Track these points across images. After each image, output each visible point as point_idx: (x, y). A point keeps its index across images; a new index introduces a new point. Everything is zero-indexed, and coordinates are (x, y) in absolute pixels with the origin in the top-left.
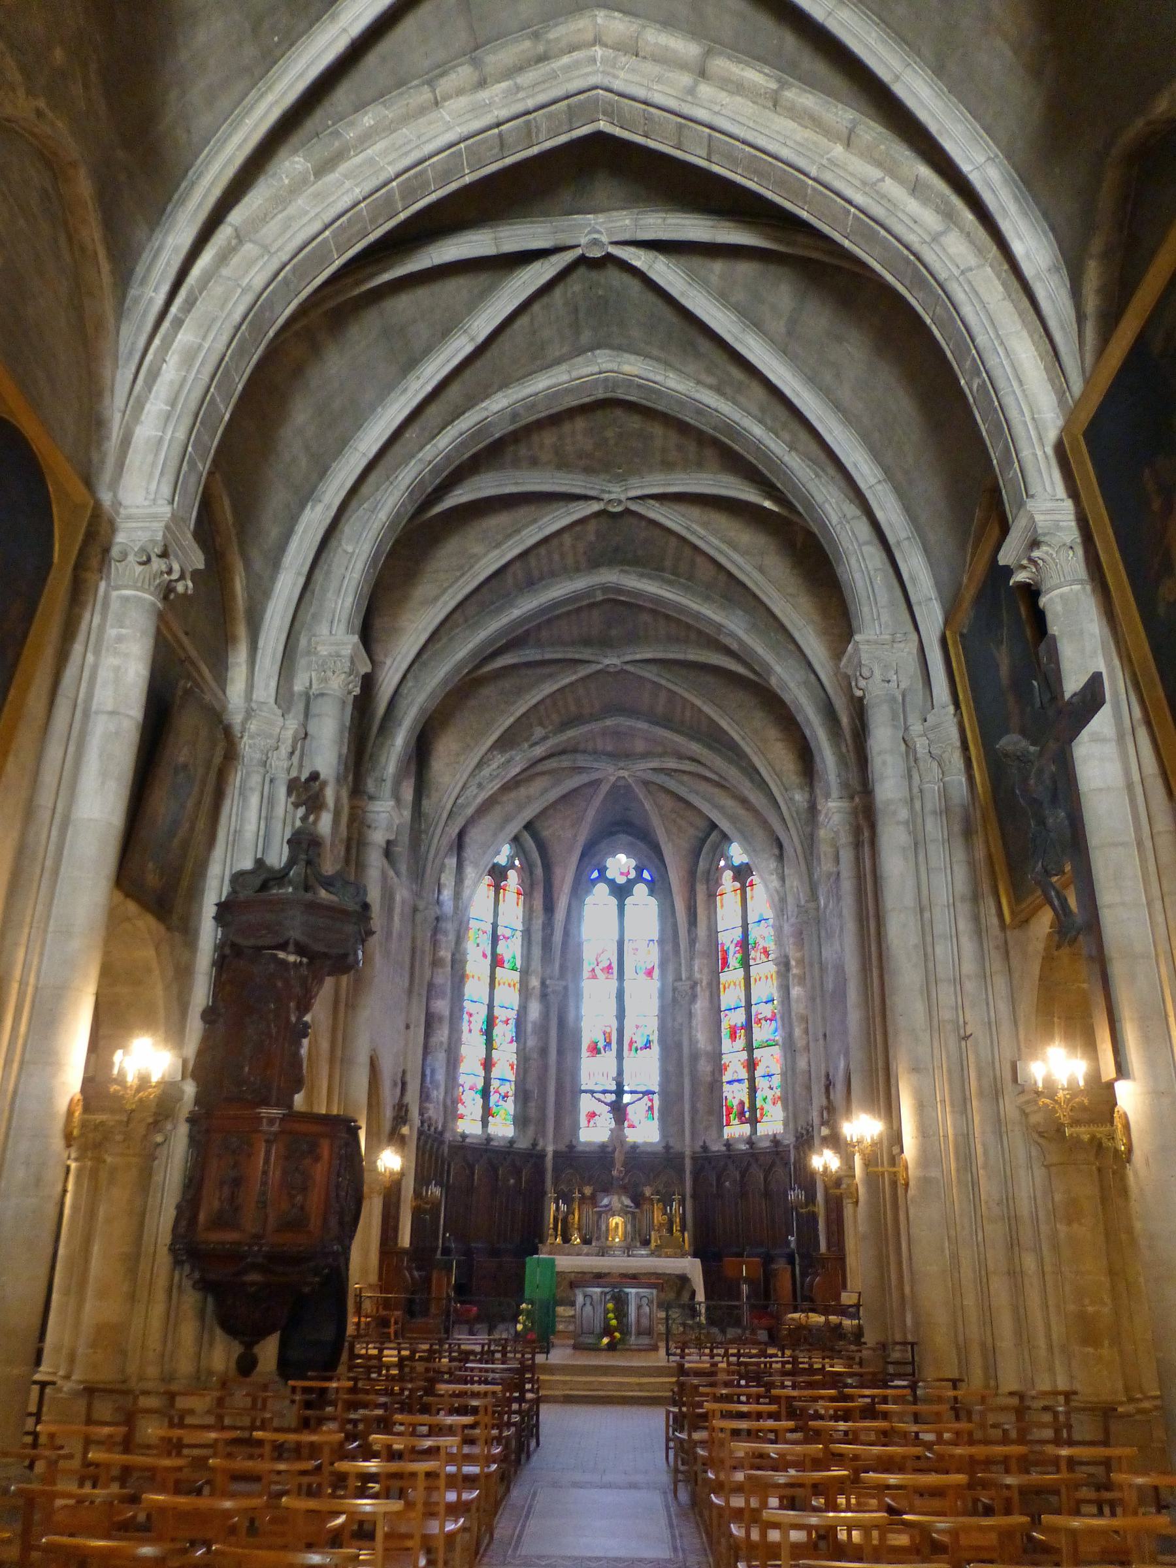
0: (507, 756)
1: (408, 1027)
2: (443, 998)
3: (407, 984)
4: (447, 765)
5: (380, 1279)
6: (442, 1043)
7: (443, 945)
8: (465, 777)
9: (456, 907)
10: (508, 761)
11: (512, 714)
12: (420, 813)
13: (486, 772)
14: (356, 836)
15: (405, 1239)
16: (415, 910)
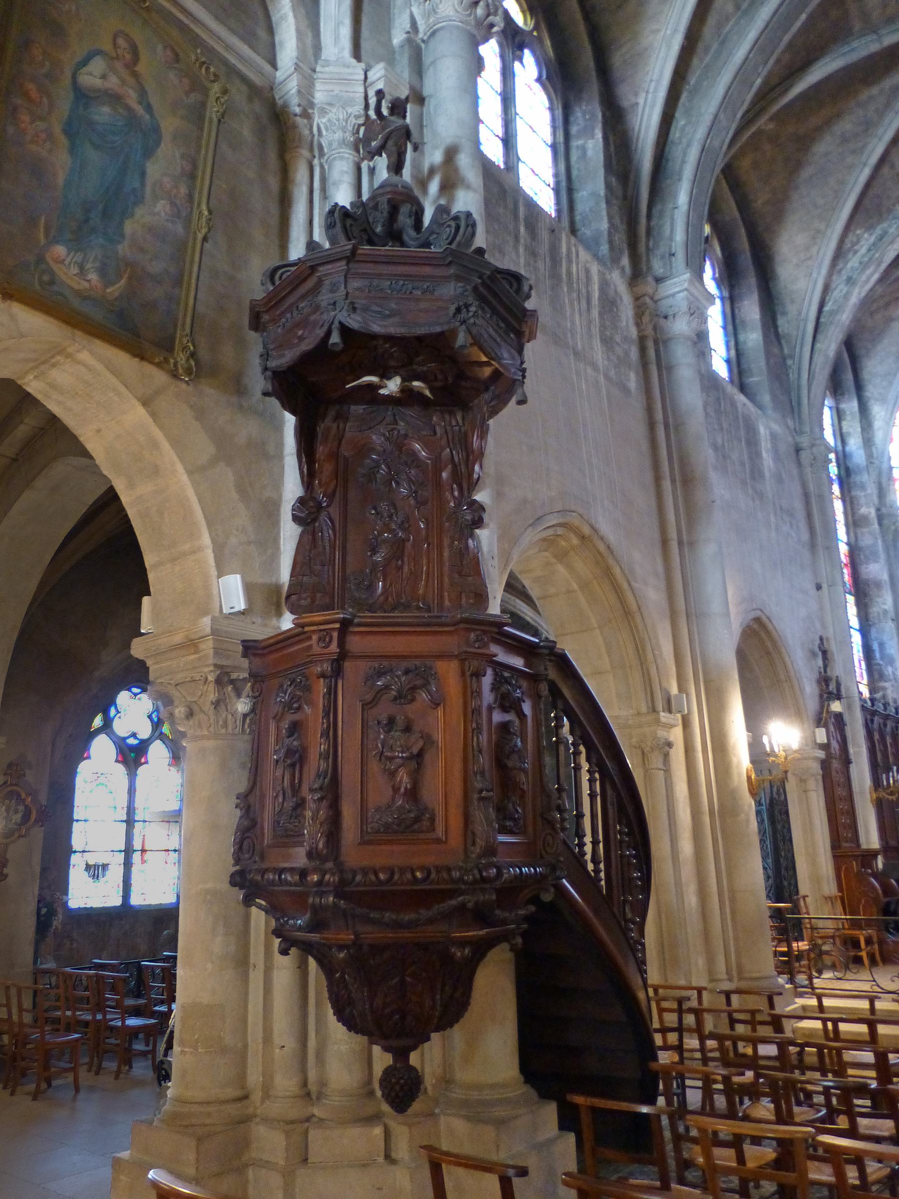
0: (878, 231)
1: (819, 587)
2: (876, 561)
3: (805, 536)
4: (798, 266)
5: (840, 889)
6: (885, 612)
7: (862, 501)
8: (824, 271)
9: (870, 456)
10: (881, 238)
11: (865, 165)
12: (777, 335)
13: (853, 262)
14: (649, 331)
15: (871, 836)
16: (798, 450)
